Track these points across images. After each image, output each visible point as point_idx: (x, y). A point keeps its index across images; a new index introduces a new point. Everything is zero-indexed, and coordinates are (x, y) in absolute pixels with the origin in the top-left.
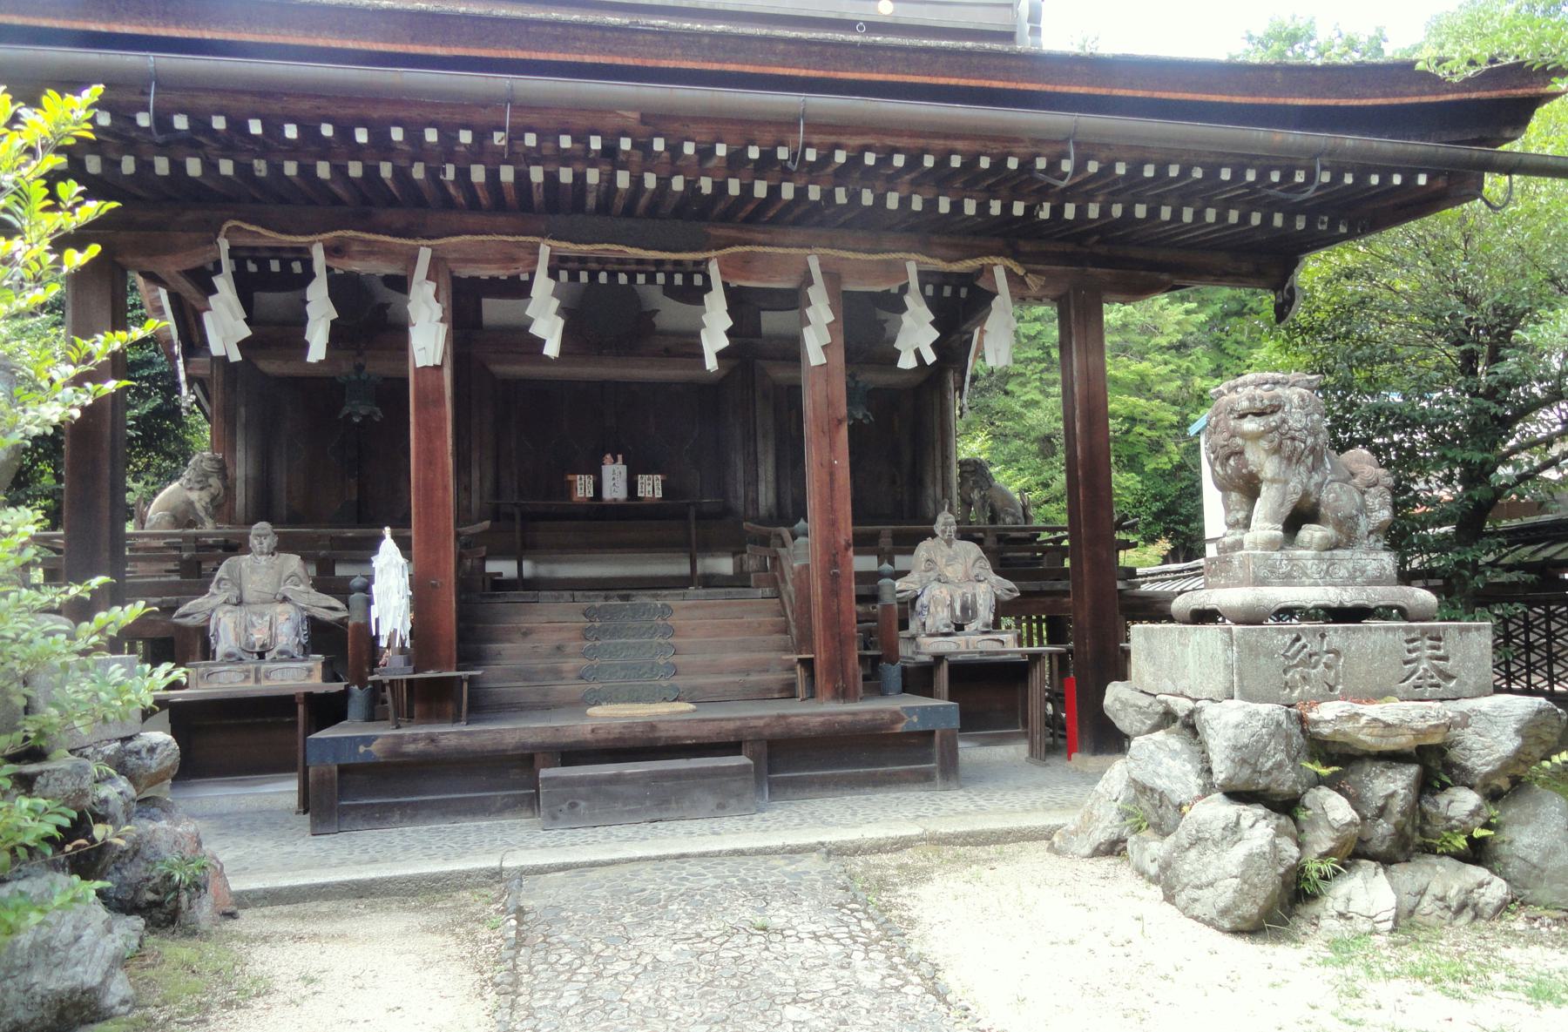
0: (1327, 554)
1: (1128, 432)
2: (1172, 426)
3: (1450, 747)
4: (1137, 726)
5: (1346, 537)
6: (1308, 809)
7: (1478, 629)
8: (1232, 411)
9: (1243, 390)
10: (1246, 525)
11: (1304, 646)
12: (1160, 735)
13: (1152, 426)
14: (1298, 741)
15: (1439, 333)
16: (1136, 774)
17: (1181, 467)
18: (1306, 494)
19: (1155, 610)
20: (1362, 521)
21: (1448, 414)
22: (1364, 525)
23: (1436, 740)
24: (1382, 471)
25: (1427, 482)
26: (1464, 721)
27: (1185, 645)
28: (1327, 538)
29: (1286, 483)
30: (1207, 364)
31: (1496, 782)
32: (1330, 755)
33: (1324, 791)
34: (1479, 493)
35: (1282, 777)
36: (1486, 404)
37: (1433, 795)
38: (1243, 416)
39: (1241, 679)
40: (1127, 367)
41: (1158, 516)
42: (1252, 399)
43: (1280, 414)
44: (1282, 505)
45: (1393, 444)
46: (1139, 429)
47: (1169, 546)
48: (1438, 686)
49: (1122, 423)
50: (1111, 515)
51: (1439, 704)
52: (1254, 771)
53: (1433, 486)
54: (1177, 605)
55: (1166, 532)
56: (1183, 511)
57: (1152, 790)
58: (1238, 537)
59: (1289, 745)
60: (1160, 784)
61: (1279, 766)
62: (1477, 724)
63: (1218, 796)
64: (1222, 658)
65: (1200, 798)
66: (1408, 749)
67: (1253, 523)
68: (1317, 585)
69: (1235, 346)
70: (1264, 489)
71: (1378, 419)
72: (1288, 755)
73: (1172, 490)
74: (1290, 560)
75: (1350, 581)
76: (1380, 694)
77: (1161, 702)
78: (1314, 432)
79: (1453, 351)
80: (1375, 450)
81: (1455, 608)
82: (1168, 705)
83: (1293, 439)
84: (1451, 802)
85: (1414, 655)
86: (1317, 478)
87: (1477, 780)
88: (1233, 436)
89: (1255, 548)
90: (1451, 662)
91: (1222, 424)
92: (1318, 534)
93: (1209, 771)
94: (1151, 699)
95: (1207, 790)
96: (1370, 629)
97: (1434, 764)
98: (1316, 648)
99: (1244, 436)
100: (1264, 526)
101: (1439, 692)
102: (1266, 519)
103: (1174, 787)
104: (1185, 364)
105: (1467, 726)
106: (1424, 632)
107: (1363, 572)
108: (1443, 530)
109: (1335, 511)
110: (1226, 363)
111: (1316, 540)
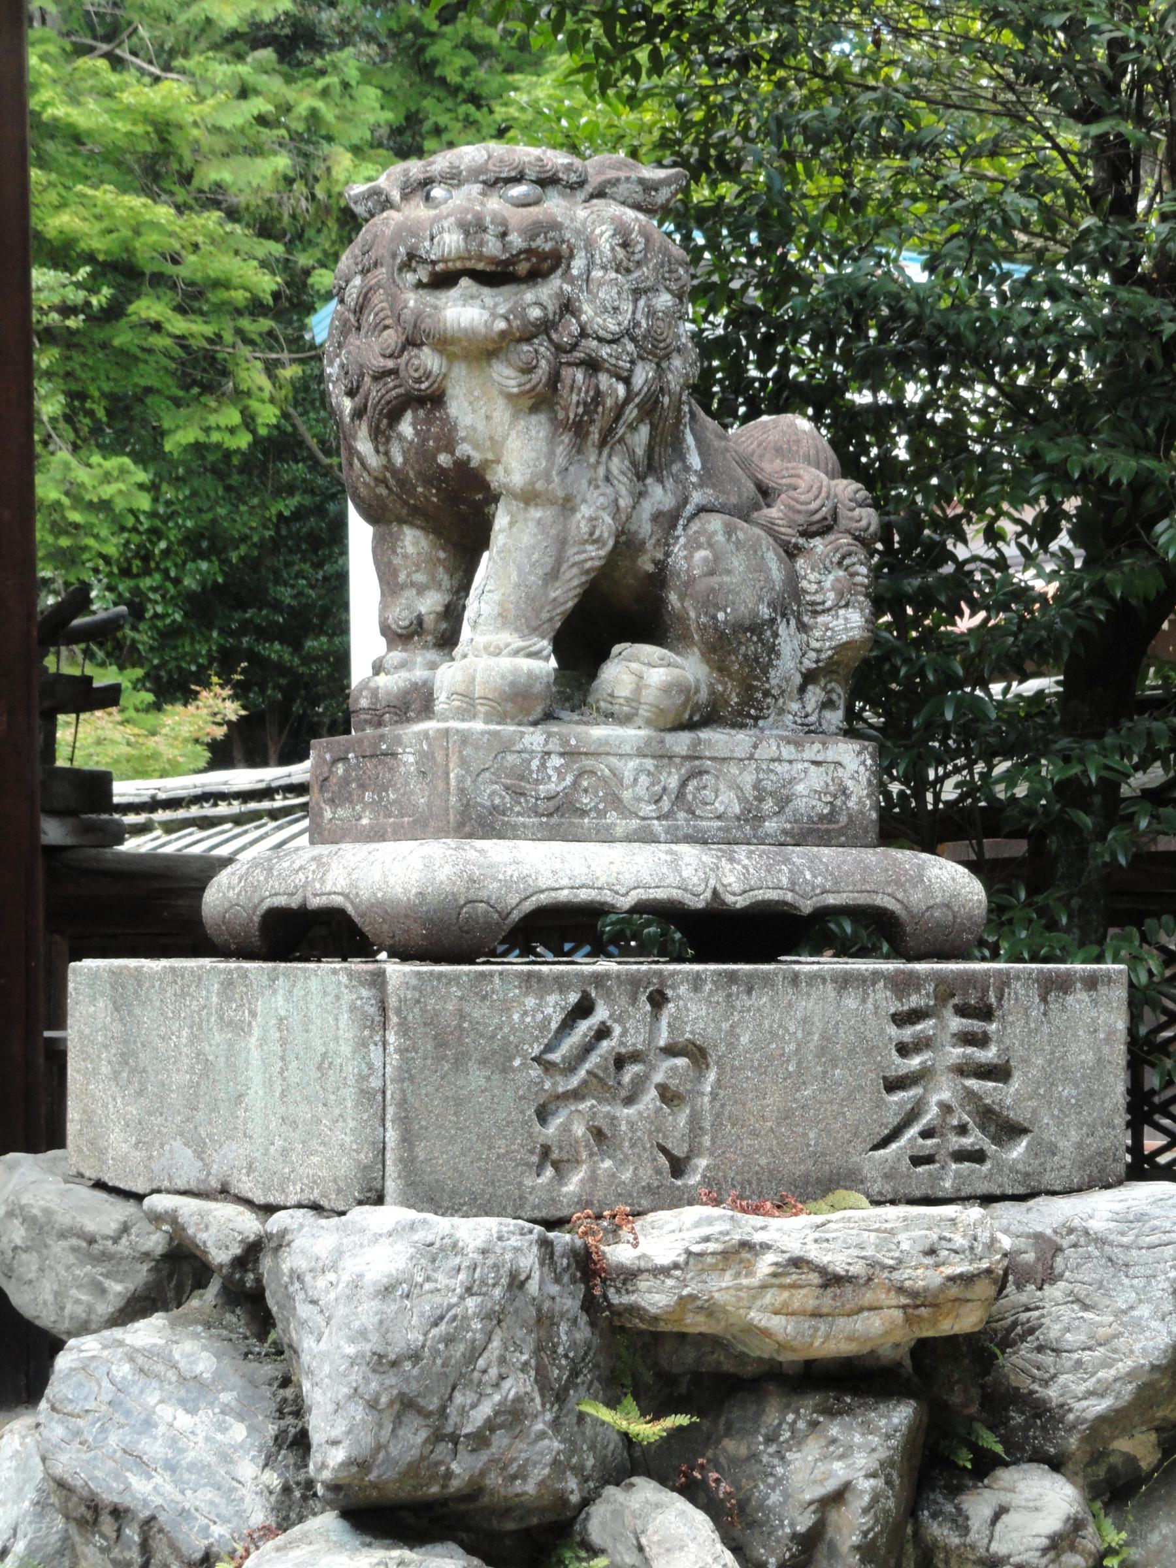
0: (681, 742)
1: (114, 312)
2: (256, 308)
3: (1007, 1341)
4: (79, 1301)
5: (735, 698)
6: (595, 1552)
7: (1091, 983)
8: (412, 259)
9: (449, 199)
10: (446, 635)
11: (603, 1032)
12: (147, 1332)
13: (192, 298)
14: (574, 1333)
15: (1035, 75)
16: (67, 1463)
17: (280, 445)
18: (626, 545)
19: (159, 914)
20: (787, 638)
21: (1051, 328)
22: (791, 653)
23: (967, 1321)
24: (847, 488)
25: (993, 536)
26: (1041, 1264)
27: (240, 1028)
28: (685, 690)
29: (568, 505)
30: (372, 110)
31: (1123, 1445)
32: (667, 1379)
33: (646, 1491)
34: (1128, 577)
35: (521, 1451)
36: (1154, 307)
37: (954, 1491)
38: (443, 280)
39: (407, 1139)
40: (108, 93)
41: (202, 607)
42: (472, 228)
43: (555, 282)
44: (553, 575)
45: (898, 410)
46: (148, 307)
47: (232, 710)
48: (978, 1156)
49: (91, 286)
50: (33, 586)
51: (975, 1212)
52: (437, 1437)
53: (1011, 551)
54: (220, 896)
55: (226, 661)
56: (285, 594)
57: (118, 1513)
58: (419, 674)
59: (544, 1348)
60: (145, 1490)
61: (512, 1416)
62: (1081, 1274)
63: (326, 1522)
64: (351, 1070)
65: (268, 1532)
66: (887, 1352)
67: (466, 632)
68: (645, 837)
69: (465, 58)
70: (501, 520)
71: (860, 330)
72: (542, 1382)
73: (250, 519)
74: (569, 754)
75: (744, 828)
76: (813, 1187)
77: (156, 1218)
78: (655, 349)
79: (1071, 137)
80: (849, 433)
81: (1052, 926)
82: (178, 1228)
83: (593, 365)
84: (1001, 1511)
85: (915, 1062)
86: (660, 496)
87: (1073, 1442)
88: (412, 342)
89: (467, 713)
90: (1016, 1084)
91: (379, 300)
92: (657, 676)
93: (301, 1443)
94: (122, 1210)
95: (292, 1505)
96: (795, 979)
97: (962, 1397)
98: (636, 1040)
99: (444, 343)
100: (499, 647)
101: (980, 1177)
102: (503, 619)
103: (189, 1500)
104: (304, 99)
105: (1051, 1277)
106: (946, 989)
107: (783, 801)
108: (1032, 686)
109: (710, 603)
110: (435, 111)
111: (650, 695)
